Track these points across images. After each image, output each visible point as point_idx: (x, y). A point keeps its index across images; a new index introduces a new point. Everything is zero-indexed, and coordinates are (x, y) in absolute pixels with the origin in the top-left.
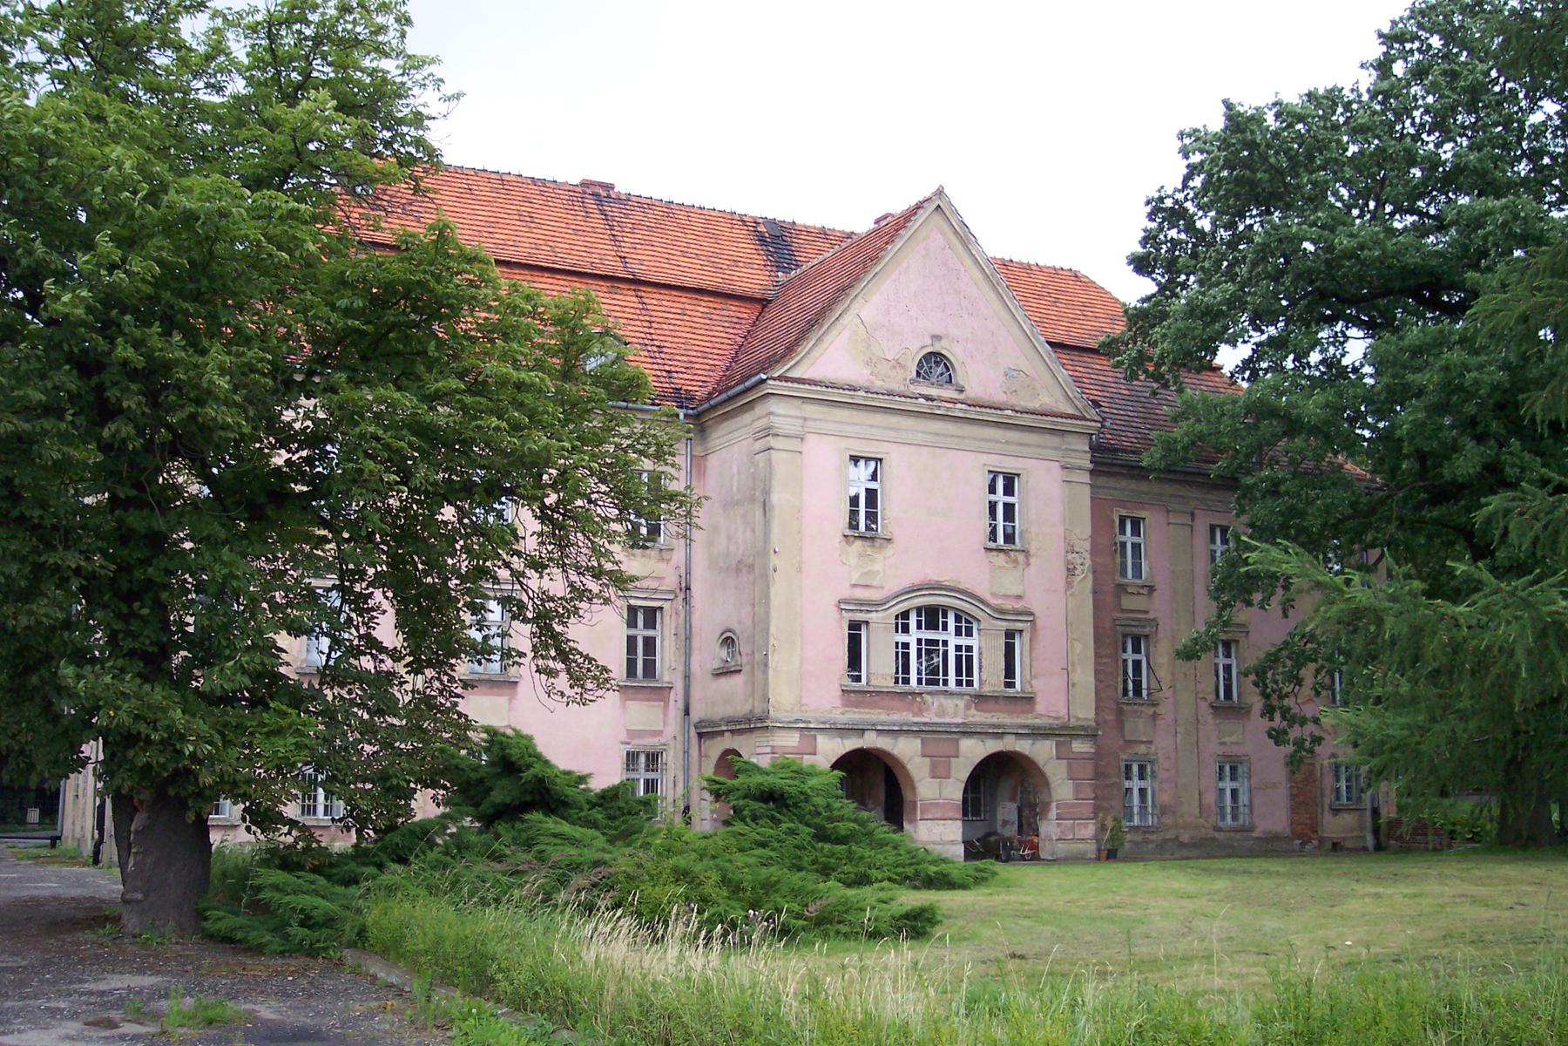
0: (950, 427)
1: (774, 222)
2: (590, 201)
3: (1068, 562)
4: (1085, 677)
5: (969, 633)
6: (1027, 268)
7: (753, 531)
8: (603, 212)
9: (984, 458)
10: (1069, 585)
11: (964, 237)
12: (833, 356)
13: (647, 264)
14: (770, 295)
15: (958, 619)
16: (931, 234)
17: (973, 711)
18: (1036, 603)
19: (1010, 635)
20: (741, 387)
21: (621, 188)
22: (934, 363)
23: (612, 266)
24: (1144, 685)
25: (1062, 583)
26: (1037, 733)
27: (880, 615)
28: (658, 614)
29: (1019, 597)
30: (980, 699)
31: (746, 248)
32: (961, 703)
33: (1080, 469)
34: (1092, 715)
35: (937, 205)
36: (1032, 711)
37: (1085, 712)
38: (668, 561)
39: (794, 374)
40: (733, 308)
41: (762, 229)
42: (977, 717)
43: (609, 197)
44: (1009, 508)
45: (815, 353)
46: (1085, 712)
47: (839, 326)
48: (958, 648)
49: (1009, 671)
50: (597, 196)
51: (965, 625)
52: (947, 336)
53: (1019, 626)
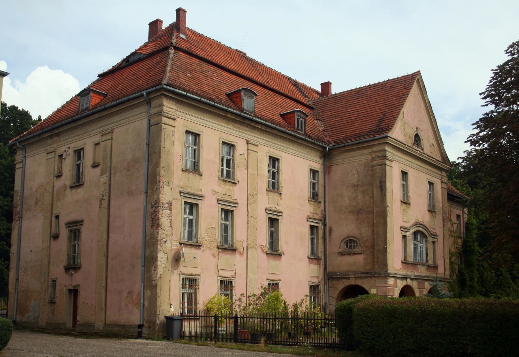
3: (443, 217)
9: (224, 135)
29: (435, 229)
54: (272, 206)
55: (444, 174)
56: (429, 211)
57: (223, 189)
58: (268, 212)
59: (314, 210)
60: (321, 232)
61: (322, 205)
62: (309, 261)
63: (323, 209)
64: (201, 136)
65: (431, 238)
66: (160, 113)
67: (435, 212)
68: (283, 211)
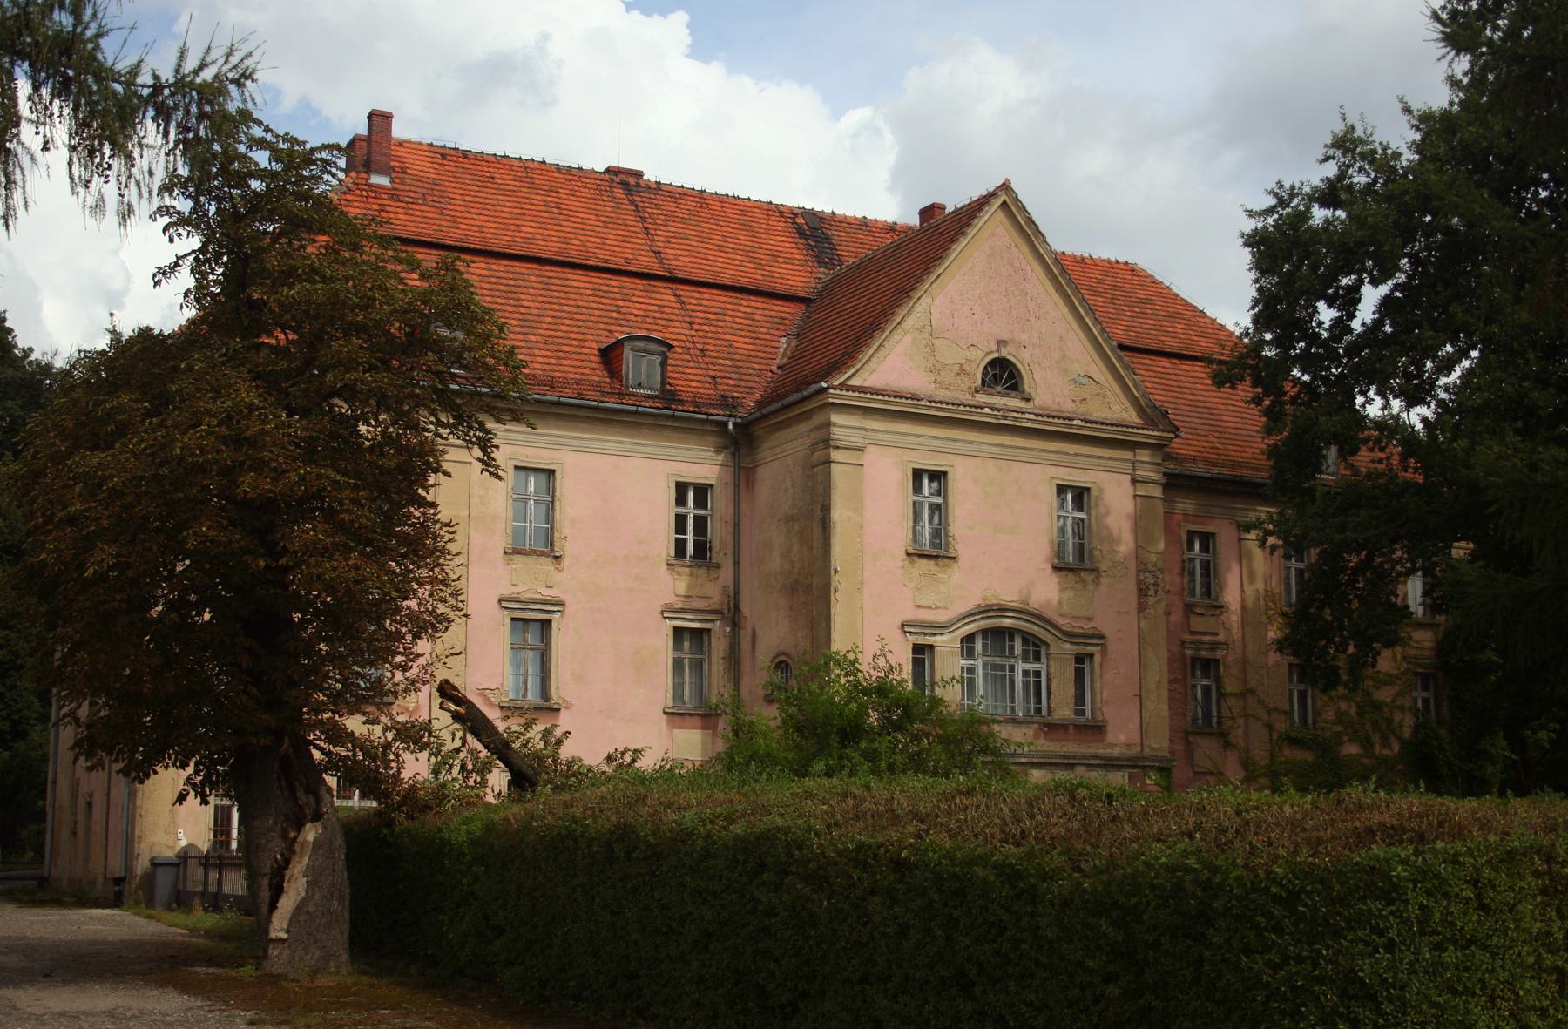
0: (1019, 441)
1: (812, 213)
2: (619, 190)
3: (1139, 582)
4: (1159, 707)
5: (1037, 659)
6: (1081, 262)
7: (811, 548)
8: (632, 202)
9: (1053, 471)
10: (1142, 607)
11: (1028, 231)
12: (893, 363)
13: (682, 260)
14: (813, 296)
15: (1025, 641)
16: (992, 228)
17: (1042, 741)
18: (1106, 624)
19: (1079, 659)
20: (797, 396)
21: (650, 176)
22: (1002, 373)
23: (647, 262)
24: (1214, 713)
25: (1134, 603)
26: (1110, 764)
27: (944, 638)
28: (706, 638)
29: (1089, 619)
30: (1053, 729)
31: (785, 242)
32: (1030, 732)
33: (1153, 482)
34: (1166, 744)
35: (1004, 200)
36: (1102, 741)
37: (1160, 743)
38: (716, 579)
39: (854, 382)
40: (779, 308)
41: (800, 220)
42: (1043, 745)
43: (638, 185)
44: (701, 523)
45: (872, 364)
46: (1160, 743)
47: (899, 330)
48: (1026, 673)
49: (1080, 699)
50: (624, 182)
51: (1035, 647)
52: (1013, 341)
53: (1090, 649)
54: (526, 589)
55: (1144, 456)
56: (1056, 569)
57: (1205, 556)
58: (505, 604)
59: (689, 587)
60: (718, 646)
61: (726, 574)
62: (668, 722)
63: (730, 583)
64: (950, 476)
65: (1068, 646)
66: (827, 443)
67: (1095, 570)
68: (563, 597)
